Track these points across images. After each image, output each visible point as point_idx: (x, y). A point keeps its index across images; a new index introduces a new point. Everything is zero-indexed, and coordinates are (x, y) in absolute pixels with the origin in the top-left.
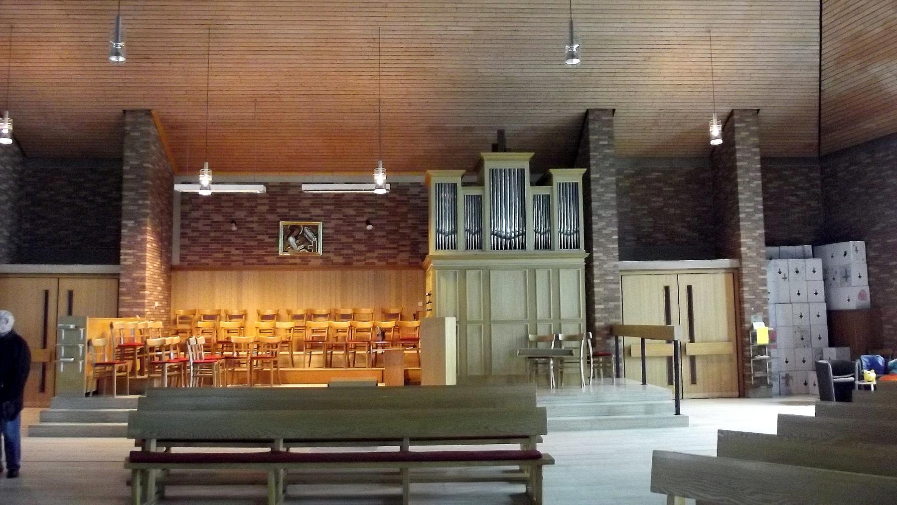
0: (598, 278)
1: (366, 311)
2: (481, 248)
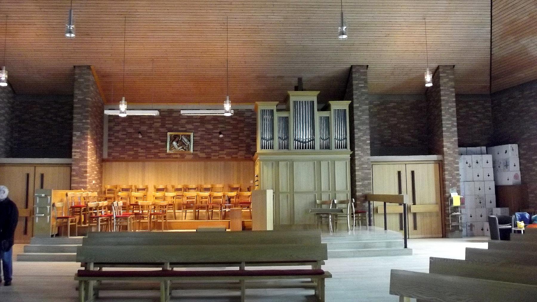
0: (358, 166)
1: (219, 186)
2: (288, 148)
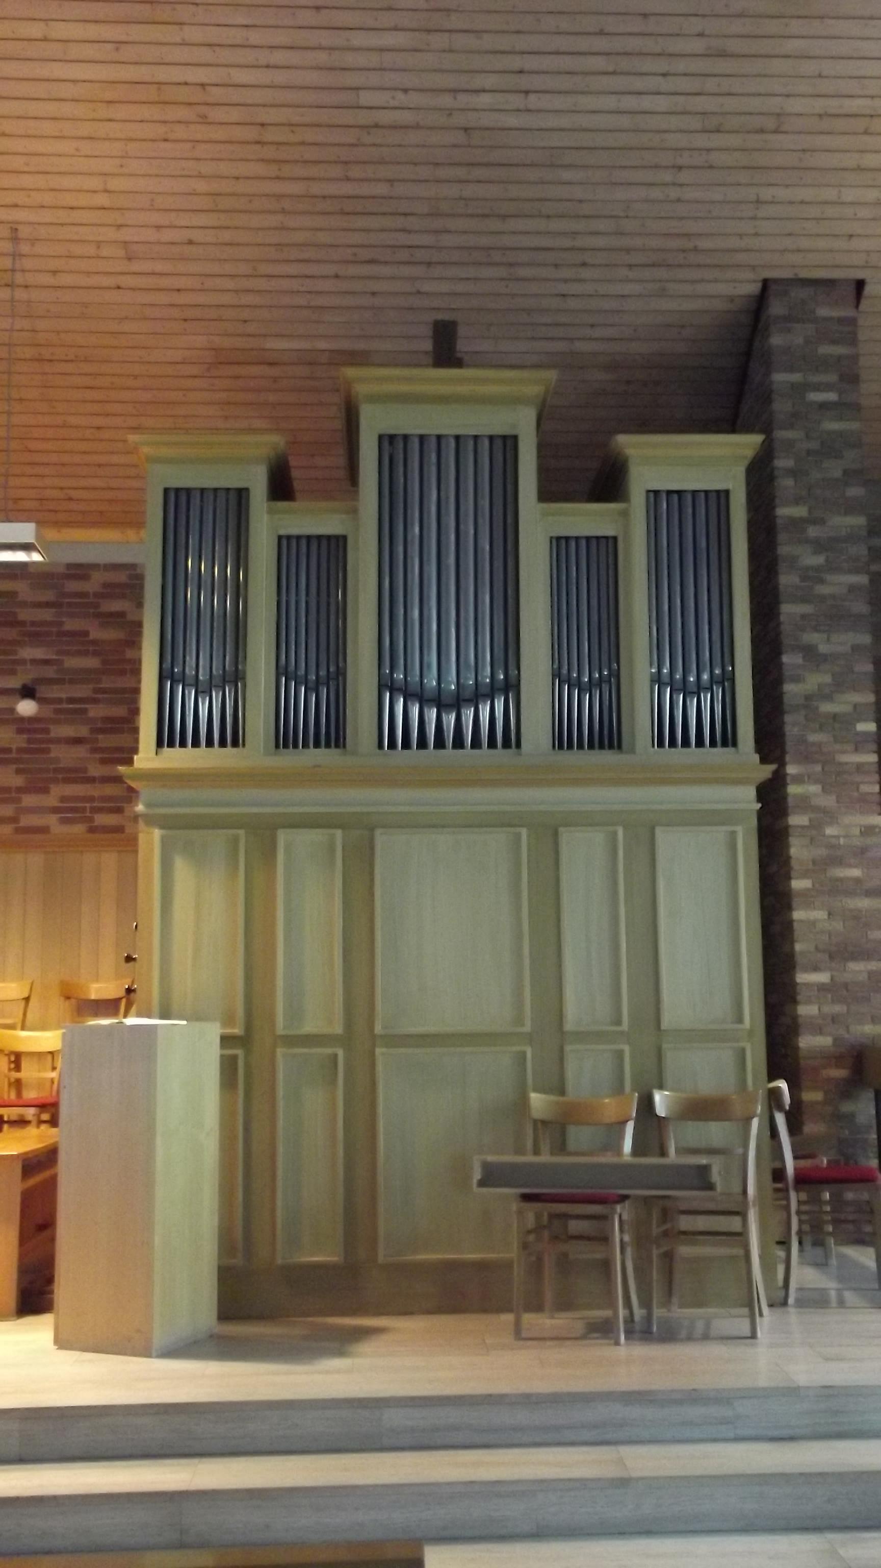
0: (804, 875)
